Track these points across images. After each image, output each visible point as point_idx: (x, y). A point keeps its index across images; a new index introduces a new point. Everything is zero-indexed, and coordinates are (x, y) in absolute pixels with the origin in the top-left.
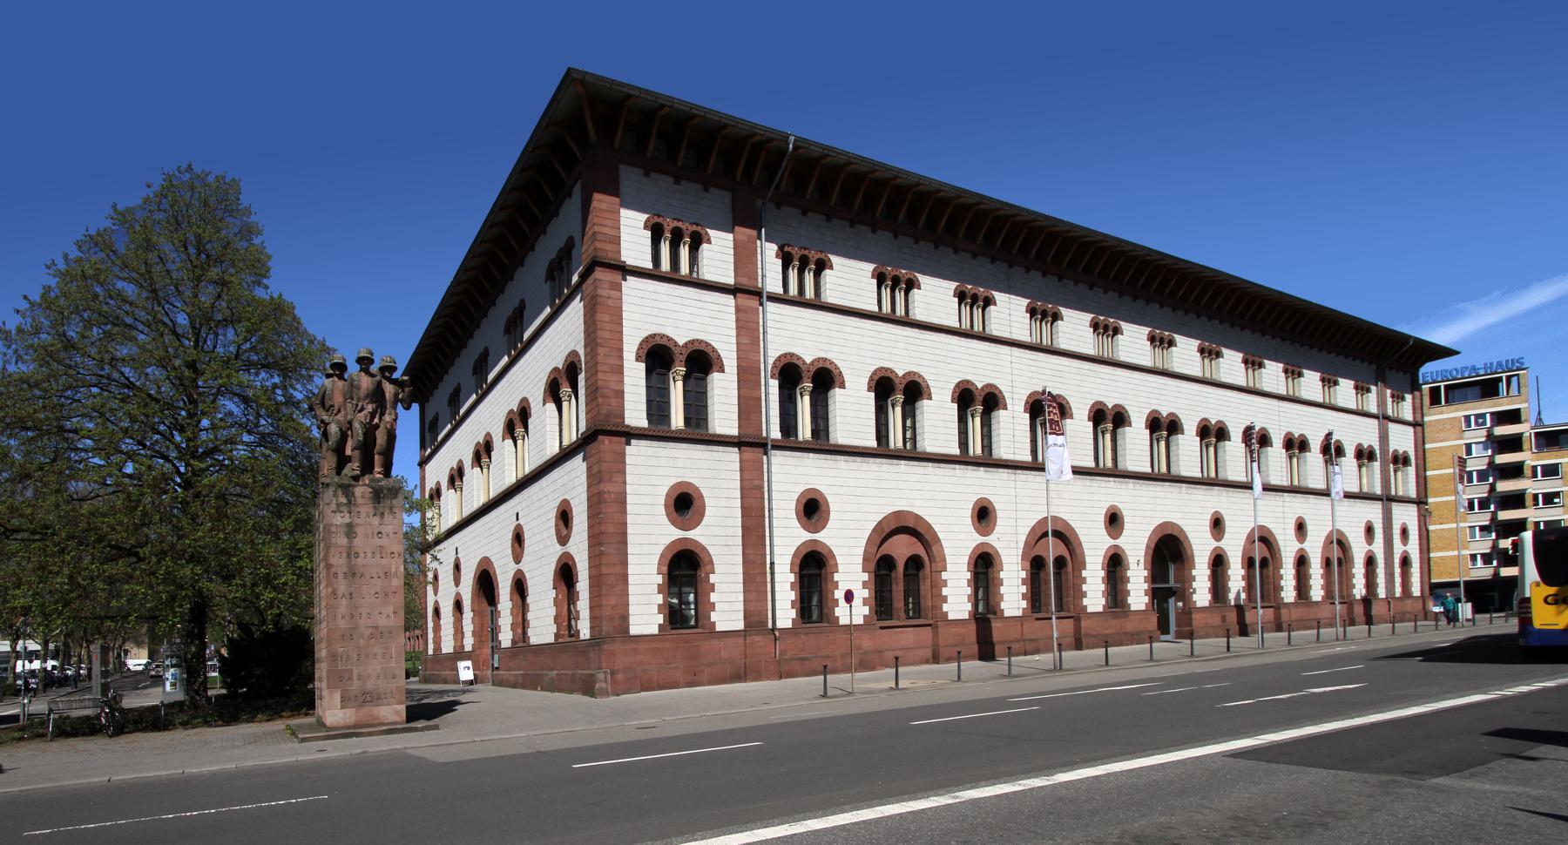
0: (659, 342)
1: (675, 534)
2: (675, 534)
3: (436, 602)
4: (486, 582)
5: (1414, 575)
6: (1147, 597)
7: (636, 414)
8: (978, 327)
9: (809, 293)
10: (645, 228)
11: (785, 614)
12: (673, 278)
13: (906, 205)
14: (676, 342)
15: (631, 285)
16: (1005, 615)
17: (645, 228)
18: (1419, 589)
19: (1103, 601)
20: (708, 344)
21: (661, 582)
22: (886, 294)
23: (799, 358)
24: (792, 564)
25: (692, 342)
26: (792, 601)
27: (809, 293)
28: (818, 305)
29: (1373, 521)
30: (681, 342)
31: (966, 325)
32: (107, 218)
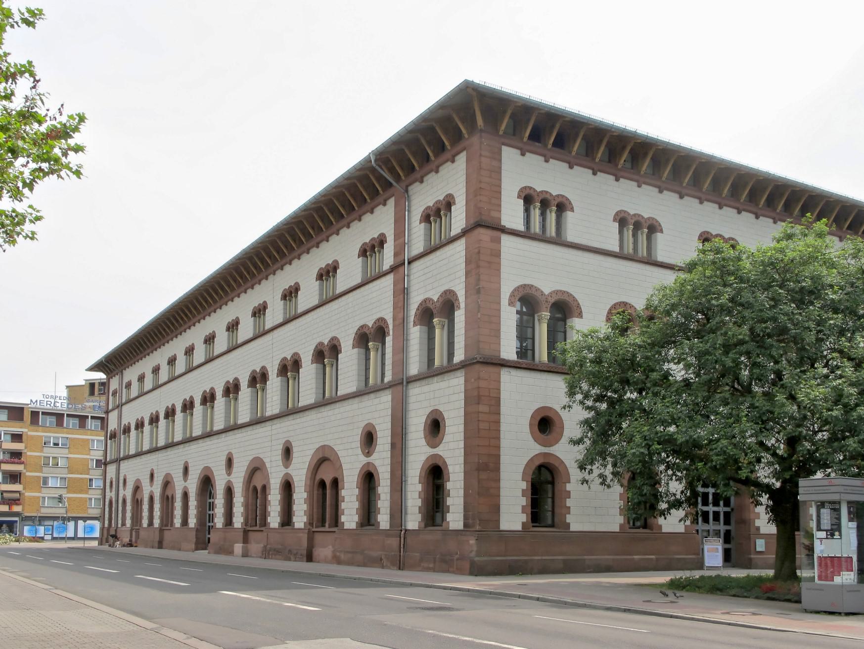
0: (533, 293)
1: (537, 449)
2: (537, 449)
3: (124, 495)
4: (207, 483)
5: (417, 495)
6: (342, 520)
7: (509, 349)
8: (643, 252)
9: (552, 231)
10: (518, 198)
11: (413, 521)
12: (542, 238)
13: (767, 193)
14: (542, 292)
15: (507, 241)
16: (663, 531)
17: (518, 198)
18: (461, 517)
19: (621, 520)
20: (569, 295)
21: (525, 488)
22: (536, 213)
23: (537, 289)
24: (524, 473)
25: (557, 292)
26: (523, 506)
27: (552, 231)
28: (559, 241)
29: (215, 387)
30: (547, 291)
31: (629, 249)
32: (78, 173)
